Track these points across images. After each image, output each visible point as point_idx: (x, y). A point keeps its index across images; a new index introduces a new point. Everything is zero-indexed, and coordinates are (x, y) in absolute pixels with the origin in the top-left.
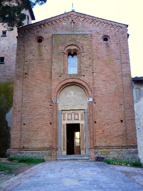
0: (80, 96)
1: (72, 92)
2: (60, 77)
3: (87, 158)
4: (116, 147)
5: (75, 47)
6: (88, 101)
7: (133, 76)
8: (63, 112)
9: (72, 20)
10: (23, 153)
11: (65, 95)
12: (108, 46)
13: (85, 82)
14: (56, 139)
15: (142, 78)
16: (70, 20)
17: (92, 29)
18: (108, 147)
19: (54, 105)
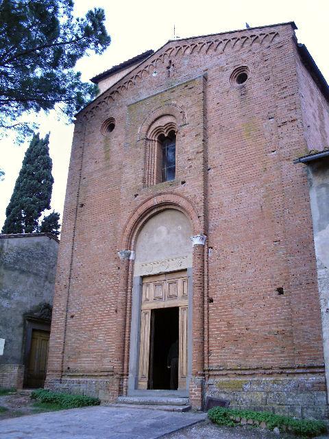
0: (180, 236)
1: (163, 229)
2: (136, 196)
4: (263, 371)
5: (167, 120)
9: (170, 62)
12: (244, 94)
13: (186, 199)
18: (241, 371)
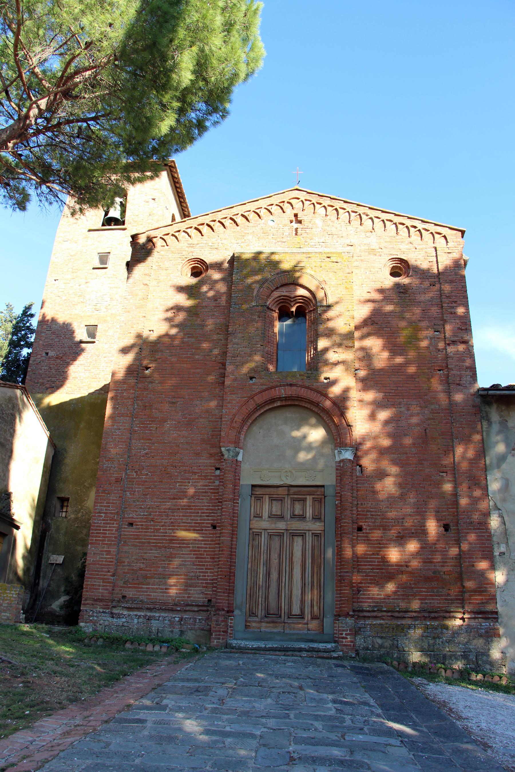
3: (329, 646)
4: (426, 615)
6: (337, 459)
7: (484, 381)
8: (259, 491)
10: (119, 616)
14: (230, 576)
15: (510, 388)
16: (290, 213)
17: (353, 240)
19: (225, 472)
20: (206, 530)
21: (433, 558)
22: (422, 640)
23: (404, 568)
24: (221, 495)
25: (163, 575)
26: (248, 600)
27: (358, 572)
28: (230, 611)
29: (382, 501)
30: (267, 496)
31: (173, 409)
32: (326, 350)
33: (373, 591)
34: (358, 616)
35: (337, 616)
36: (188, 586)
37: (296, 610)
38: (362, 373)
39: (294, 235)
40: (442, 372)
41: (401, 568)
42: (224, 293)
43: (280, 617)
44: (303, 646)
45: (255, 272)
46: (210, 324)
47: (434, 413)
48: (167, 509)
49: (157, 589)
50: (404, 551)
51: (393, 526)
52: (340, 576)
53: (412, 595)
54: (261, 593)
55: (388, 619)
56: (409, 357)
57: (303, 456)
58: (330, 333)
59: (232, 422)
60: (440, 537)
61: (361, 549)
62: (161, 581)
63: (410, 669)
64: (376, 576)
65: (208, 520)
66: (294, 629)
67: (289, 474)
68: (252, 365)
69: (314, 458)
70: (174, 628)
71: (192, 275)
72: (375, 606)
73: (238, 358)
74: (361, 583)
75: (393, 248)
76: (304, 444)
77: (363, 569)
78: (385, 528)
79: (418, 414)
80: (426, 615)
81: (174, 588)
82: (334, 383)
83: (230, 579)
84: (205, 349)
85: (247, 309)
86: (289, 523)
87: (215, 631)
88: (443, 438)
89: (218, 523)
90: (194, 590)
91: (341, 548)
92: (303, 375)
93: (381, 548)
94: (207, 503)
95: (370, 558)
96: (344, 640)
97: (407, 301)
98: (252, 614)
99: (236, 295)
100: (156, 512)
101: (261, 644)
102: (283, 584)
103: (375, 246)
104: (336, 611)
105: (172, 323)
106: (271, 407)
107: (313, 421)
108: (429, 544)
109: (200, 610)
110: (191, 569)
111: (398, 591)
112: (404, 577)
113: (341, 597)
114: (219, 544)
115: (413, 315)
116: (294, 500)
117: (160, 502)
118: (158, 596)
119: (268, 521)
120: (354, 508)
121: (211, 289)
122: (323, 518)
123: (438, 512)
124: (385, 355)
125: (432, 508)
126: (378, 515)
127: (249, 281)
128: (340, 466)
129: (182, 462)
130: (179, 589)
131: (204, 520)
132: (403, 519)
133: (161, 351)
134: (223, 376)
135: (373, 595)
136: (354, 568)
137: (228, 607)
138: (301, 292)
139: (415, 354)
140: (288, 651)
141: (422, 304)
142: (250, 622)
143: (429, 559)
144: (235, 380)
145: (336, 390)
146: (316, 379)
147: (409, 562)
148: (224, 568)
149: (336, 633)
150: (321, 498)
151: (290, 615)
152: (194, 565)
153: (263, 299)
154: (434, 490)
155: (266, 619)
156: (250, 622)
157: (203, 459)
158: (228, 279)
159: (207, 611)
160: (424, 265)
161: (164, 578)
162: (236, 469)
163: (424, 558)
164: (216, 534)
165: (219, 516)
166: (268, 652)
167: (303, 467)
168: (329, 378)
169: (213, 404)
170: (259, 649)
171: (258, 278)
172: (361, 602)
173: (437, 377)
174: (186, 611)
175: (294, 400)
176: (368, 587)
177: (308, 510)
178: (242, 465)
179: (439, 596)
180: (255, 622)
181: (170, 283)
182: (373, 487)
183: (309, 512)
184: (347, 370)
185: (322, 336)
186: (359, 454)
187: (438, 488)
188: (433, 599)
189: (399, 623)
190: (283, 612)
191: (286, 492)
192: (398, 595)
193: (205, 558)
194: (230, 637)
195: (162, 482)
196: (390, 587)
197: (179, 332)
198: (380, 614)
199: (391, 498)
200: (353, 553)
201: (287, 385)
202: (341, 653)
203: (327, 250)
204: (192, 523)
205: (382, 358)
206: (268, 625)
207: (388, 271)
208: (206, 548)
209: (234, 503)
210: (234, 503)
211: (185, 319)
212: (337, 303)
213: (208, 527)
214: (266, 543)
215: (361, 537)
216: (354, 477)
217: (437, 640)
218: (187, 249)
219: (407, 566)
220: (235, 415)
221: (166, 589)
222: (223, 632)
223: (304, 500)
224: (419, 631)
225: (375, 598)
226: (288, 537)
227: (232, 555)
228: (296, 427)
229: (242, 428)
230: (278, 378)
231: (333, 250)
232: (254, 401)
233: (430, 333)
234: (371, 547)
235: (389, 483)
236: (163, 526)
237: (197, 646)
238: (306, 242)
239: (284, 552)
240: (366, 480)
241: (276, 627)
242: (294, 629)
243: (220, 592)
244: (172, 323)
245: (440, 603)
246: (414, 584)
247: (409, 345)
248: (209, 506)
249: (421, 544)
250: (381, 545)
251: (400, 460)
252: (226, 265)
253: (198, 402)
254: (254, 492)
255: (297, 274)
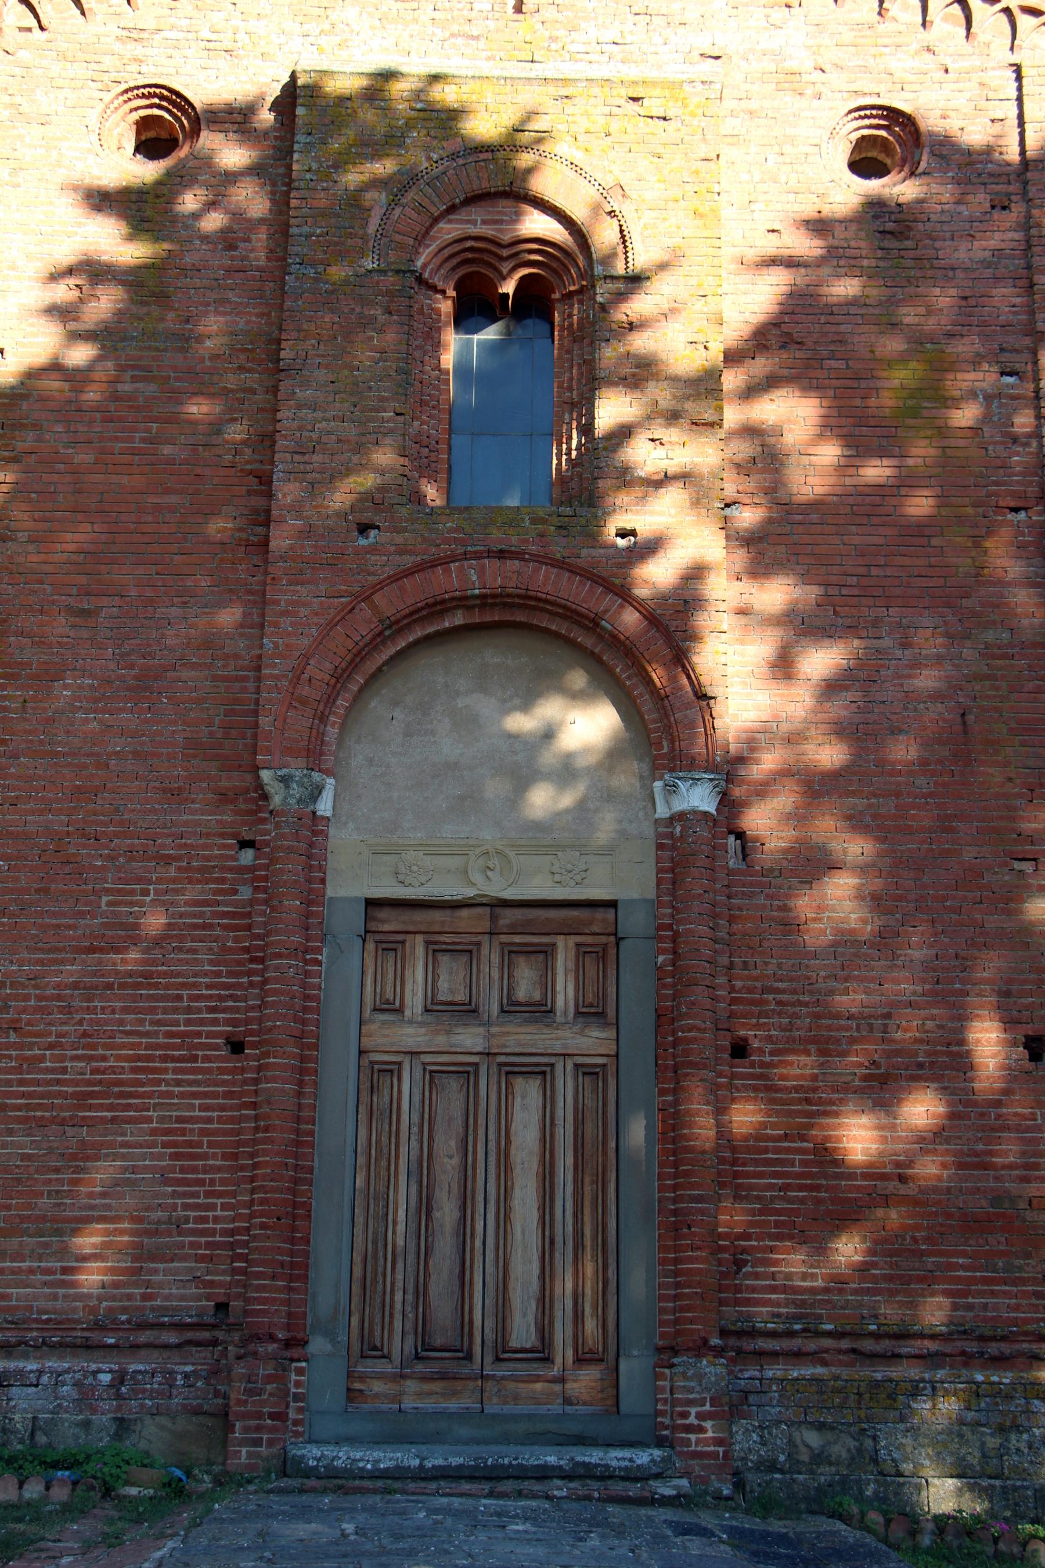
3: (643, 1457)
4: (972, 1347)
6: (662, 811)
8: (390, 922)
11: (408, 734)
14: (295, 1218)
20: (207, 1059)
21: (991, 1153)
22: (961, 1436)
23: (892, 1186)
24: (258, 937)
25: (54, 1220)
26: (355, 1300)
27: (737, 1198)
28: (295, 1343)
29: (815, 955)
30: (420, 939)
31: (85, 634)
32: (624, 433)
33: (789, 1264)
34: (739, 1351)
35: (667, 1352)
36: (142, 1257)
37: (523, 1332)
38: (748, 517)
39: (510, 10)
40: (1022, 515)
41: (886, 1180)
42: (262, 221)
43: (469, 1357)
44: (552, 1459)
45: (372, 147)
46: (214, 330)
47: (994, 657)
48: (67, 986)
49: (31, 1271)
50: (893, 1127)
51: (853, 1041)
52: (675, 1213)
53: (921, 1280)
54: (399, 1276)
55: (841, 1363)
56: (910, 462)
57: (542, 800)
58: (640, 373)
59: (296, 681)
60: (1013, 1076)
61: (745, 1116)
62: (47, 1245)
63: (926, 1541)
64: (796, 1212)
65: (215, 1022)
66: (516, 1398)
67: (495, 862)
68: (368, 481)
69: (581, 806)
70: (94, 1410)
71: (138, 150)
72: (797, 1318)
73: (317, 458)
74: (747, 1236)
75: (865, 69)
76: (547, 759)
77: (752, 1187)
78: (826, 1047)
79: (939, 660)
80: (972, 1347)
81: (95, 1264)
82: (651, 547)
83: (294, 1229)
84: (194, 423)
85: (346, 282)
86: (494, 1030)
87: (245, 1416)
88: (1023, 744)
89: (251, 1033)
90: (166, 1272)
91: (676, 1115)
92: (543, 521)
93: (812, 1115)
94: (211, 962)
95: (777, 1150)
96: (693, 1437)
97: (910, 263)
98: (372, 1350)
99: (306, 229)
100: (27, 998)
101: (408, 1458)
102: (478, 1243)
103: (802, 61)
104: (663, 1335)
105: (73, 326)
106: (431, 629)
107: (578, 679)
108: (975, 1104)
109: (189, 1342)
110: (157, 1195)
111: (875, 1265)
112: (893, 1214)
113: (678, 1285)
114: (254, 1105)
115: (929, 313)
116: (511, 953)
117: (41, 962)
118: (36, 1297)
119: (421, 1024)
120: (721, 980)
121: (211, 205)
122: (611, 1012)
123: (1007, 994)
124: (830, 453)
125: (986, 981)
126: (800, 1003)
127: (353, 178)
128: (671, 835)
129: (121, 823)
130: (112, 1271)
131: (202, 1022)
132: (888, 1016)
133: (36, 426)
134: (264, 519)
135: (789, 1276)
136: (722, 1185)
137: (288, 1327)
138: (536, 224)
139: (932, 452)
140: (499, 1479)
141: (960, 274)
142: (362, 1378)
143: (976, 1154)
144: (308, 532)
145: (658, 574)
146: (592, 533)
147: (910, 1164)
148: (275, 1190)
149: (663, 1413)
150: (605, 947)
151: (502, 1352)
152: (167, 1182)
153: (401, 246)
154: (993, 921)
155: (419, 1367)
156: (362, 1378)
157: (193, 812)
158: (275, 168)
159: (214, 1343)
160: (974, 134)
161: (58, 1232)
162: (311, 845)
163: (961, 1153)
164: (243, 1070)
165: (252, 1008)
166: (433, 1486)
167: (543, 839)
168: (633, 533)
169: (229, 617)
170: (398, 1474)
171: (384, 167)
172: (748, 1302)
173: (1005, 534)
174: (136, 1347)
175: (511, 606)
176: (772, 1249)
177: (559, 987)
178: (332, 832)
179: (1014, 1282)
180: (381, 1377)
181: (62, 175)
182: (785, 908)
183: (565, 994)
184: (696, 503)
185: (611, 383)
186: (737, 792)
187: (1008, 912)
188: (993, 1294)
189: (879, 1376)
190: (478, 1340)
191: (486, 925)
192: (875, 1279)
193: (205, 1157)
194: (297, 1434)
195: (45, 891)
196: (848, 1249)
197: (99, 358)
198: (812, 1346)
199: (845, 943)
200: (720, 1134)
201: (490, 554)
202: (684, 1482)
203: (631, 72)
204: (156, 1034)
205: (816, 464)
206: (427, 1387)
207: (841, 153)
208: (209, 1120)
209: (306, 962)
210: (306, 962)
211: (119, 314)
212: (663, 266)
213: (216, 1047)
214: (417, 1099)
215: (743, 1076)
216: (721, 874)
217: (1013, 1437)
218: (117, 47)
219: (902, 1179)
220: (306, 658)
221: (65, 1270)
222: (272, 1416)
223: (547, 952)
224: (949, 1406)
225: (796, 1290)
226: (494, 1080)
227: (301, 1143)
228: (517, 701)
229: (330, 700)
230: (459, 529)
231: (653, 74)
232: (374, 607)
233: (986, 377)
234: (778, 1113)
235: (839, 893)
236: (51, 1047)
237: (179, 1473)
238: (553, 39)
239: (481, 1132)
240: (760, 884)
241: (454, 1393)
242: (516, 1398)
243: (259, 1275)
244: (73, 326)
245: (1017, 1308)
246: (928, 1240)
247: (910, 422)
248: (218, 974)
249: (949, 1104)
250: (815, 1104)
251: (874, 817)
252: (266, 117)
253: (175, 612)
254: (373, 926)
255: (525, 159)
